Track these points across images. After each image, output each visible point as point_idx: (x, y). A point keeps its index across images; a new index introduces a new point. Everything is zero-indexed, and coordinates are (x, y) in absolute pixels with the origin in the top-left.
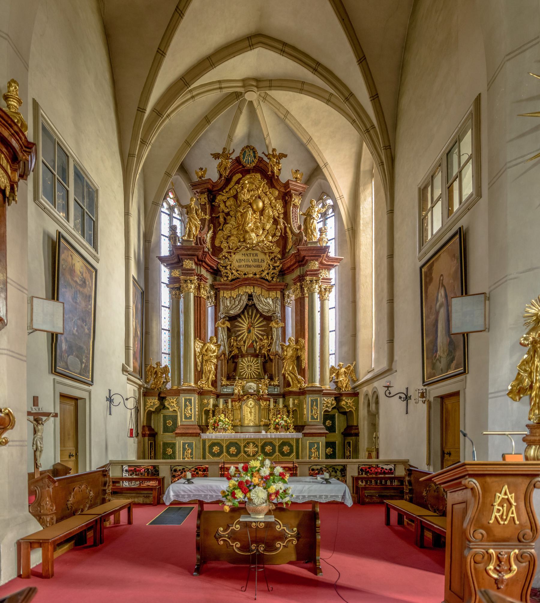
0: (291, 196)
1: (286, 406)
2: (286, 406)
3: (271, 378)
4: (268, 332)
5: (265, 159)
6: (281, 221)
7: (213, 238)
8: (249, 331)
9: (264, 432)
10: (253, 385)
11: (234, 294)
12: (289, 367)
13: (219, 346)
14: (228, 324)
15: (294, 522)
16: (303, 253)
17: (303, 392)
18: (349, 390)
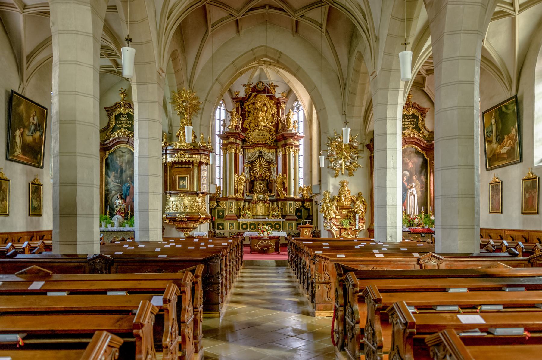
0: (280, 104)
1: (278, 206)
2: (278, 206)
3: (271, 192)
4: (269, 169)
5: (268, 86)
6: (276, 116)
7: (242, 124)
8: (260, 168)
9: (267, 218)
10: (262, 196)
11: (253, 151)
12: (279, 187)
13: (245, 176)
14: (250, 165)
15: (274, 242)
16: (285, 136)
17: (285, 200)
18: (308, 198)
